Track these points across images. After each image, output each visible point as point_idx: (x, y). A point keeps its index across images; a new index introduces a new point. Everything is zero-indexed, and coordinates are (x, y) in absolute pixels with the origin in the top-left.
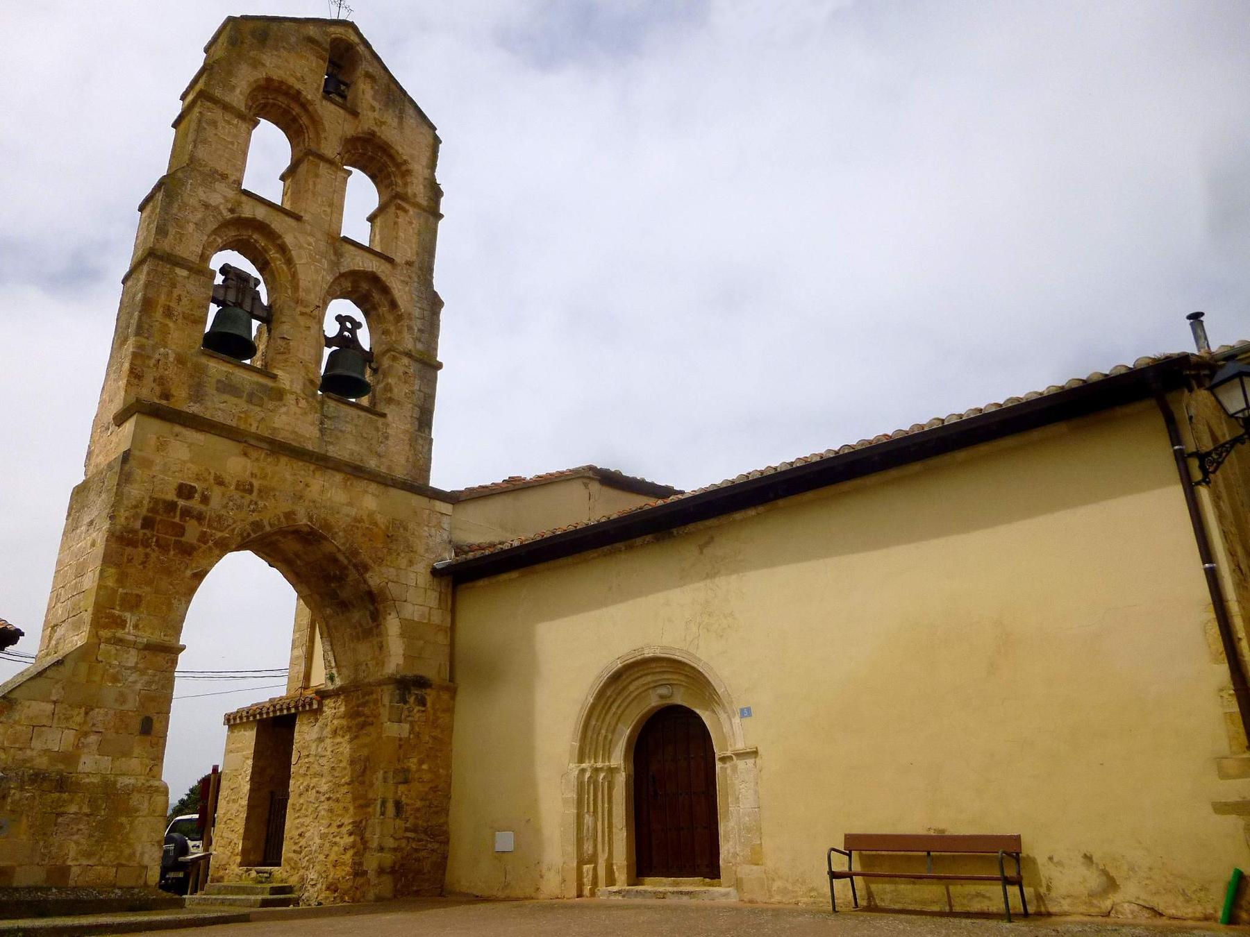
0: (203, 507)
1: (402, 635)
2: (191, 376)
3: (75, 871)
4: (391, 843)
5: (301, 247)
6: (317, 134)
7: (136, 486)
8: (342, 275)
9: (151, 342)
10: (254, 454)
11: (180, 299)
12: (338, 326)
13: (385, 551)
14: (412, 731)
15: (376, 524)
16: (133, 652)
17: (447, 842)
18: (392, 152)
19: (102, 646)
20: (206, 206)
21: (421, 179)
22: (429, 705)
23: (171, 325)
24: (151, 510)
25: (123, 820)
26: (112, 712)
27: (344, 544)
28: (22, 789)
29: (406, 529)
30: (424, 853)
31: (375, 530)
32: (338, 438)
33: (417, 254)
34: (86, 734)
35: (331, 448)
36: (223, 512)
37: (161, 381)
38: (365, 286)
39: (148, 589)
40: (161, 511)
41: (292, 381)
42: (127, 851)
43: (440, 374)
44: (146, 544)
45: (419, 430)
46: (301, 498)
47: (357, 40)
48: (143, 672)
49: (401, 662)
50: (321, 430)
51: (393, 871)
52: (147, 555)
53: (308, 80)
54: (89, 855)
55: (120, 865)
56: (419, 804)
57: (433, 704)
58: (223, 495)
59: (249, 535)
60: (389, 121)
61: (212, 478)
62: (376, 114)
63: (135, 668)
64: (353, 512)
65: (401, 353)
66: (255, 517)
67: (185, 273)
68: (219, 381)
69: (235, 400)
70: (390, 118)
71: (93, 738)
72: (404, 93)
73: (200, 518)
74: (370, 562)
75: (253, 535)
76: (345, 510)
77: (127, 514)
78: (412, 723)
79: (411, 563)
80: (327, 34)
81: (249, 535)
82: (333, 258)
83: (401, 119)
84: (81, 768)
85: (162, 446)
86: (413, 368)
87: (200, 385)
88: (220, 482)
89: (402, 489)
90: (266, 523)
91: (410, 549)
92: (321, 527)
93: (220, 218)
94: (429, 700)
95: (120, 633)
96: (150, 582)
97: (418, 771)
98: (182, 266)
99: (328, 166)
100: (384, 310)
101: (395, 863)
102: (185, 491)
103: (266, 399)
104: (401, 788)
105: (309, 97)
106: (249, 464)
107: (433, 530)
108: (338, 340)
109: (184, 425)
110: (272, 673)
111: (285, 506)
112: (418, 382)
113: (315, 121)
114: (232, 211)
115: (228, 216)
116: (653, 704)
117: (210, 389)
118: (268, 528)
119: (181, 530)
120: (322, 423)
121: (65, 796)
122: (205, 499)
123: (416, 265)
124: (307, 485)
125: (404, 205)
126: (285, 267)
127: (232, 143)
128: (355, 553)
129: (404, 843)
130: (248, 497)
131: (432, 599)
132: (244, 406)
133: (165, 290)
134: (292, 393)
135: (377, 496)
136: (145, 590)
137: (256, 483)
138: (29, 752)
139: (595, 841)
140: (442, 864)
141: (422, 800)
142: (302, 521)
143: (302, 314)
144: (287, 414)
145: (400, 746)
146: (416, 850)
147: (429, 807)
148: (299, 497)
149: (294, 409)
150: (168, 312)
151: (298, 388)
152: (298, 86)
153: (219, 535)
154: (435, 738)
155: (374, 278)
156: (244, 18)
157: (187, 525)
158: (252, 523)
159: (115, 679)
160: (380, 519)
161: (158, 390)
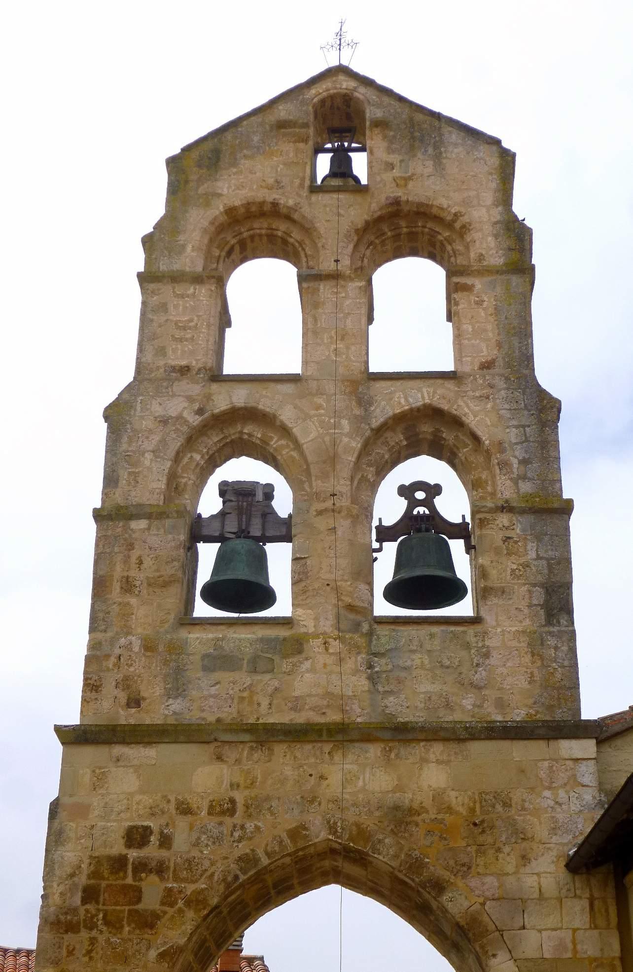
0: (164, 853)
2: (166, 663)
6: (315, 245)
7: (70, 846)
8: (379, 431)
9: (109, 634)
10: (231, 754)
11: (140, 563)
12: (403, 503)
13: (472, 849)
15: (449, 809)
18: (434, 211)
20: (164, 421)
21: (487, 228)
24: (95, 874)
27: (396, 856)
29: (507, 805)
32: (399, 681)
33: (499, 345)
36: (195, 853)
37: (126, 683)
38: (426, 429)
41: (316, 619)
43: (575, 522)
44: (91, 925)
45: (549, 623)
46: (312, 802)
47: (352, 84)
50: (370, 678)
52: (93, 941)
53: (285, 181)
58: (191, 828)
59: (236, 877)
60: (419, 170)
61: (172, 807)
62: (396, 173)
65: (491, 511)
66: (243, 848)
67: (142, 524)
68: (205, 656)
69: (236, 675)
70: (422, 165)
73: (160, 870)
74: (446, 875)
75: (242, 878)
77: (61, 888)
79: (525, 859)
80: (303, 103)
81: (236, 877)
82: (357, 412)
83: (438, 159)
85: (100, 779)
86: (519, 526)
87: (179, 671)
88: (185, 809)
90: (260, 853)
91: (521, 836)
92: (351, 839)
93: (185, 429)
102: (137, 837)
103: (277, 659)
105: (291, 203)
109: (124, 742)
111: (289, 820)
112: (532, 546)
113: (307, 229)
114: (200, 412)
115: (195, 420)
117: (194, 673)
118: (265, 861)
119: (136, 894)
120: (370, 667)
122: (166, 841)
123: (500, 362)
124: (322, 777)
125: (468, 281)
126: (294, 454)
130: (228, 821)
132: (245, 679)
133: (119, 558)
134: (316, 636)
142: (319, 834)
143: (320, 513)
144: (312, 670)
148: (312, 799)
149: (322, 659)
150: (128, 586)
151: (327, 625)
153: (190, 888)
155: (434, 413)
156: (187, 149)
158: (240, 858)
160: (455, 798)
161: (123, 697)
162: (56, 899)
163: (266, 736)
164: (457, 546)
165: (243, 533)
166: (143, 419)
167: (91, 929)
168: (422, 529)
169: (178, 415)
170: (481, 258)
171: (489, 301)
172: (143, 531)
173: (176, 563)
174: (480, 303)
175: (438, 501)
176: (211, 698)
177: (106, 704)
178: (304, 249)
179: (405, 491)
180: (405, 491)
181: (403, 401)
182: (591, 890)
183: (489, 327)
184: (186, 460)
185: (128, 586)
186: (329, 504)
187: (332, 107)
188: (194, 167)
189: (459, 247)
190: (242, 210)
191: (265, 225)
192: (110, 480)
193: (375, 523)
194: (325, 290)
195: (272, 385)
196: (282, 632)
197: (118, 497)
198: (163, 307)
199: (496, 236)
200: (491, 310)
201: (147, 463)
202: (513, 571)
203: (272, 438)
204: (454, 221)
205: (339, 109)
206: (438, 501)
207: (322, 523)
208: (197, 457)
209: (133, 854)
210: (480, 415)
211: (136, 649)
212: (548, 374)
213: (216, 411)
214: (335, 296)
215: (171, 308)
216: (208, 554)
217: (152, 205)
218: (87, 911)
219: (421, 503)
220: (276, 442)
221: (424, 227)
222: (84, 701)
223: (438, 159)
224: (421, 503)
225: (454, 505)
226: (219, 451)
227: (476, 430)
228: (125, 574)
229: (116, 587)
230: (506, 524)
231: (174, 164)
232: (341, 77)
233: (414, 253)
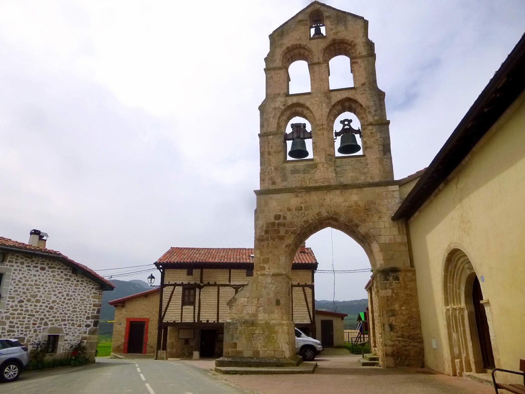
0: (284, 221)
1: (381, 251)
2: (281, 173)
3: (261, 352)
4: (390, 343)
5: (313, 104)
6: (312, 55)
8: (334, 106)
12: (342, 125)
14: (393, 292)
15: (359, 206)
16: (269, 277)
17: (422, 342)
18: (345, 41)
21: (361, 44)
22: (401, 279)
23: (271, 157)
24: (267, 227)
25: (274, 335)
26: (266, 299)
27: (345, 219)
28: (241, 326)
29: (375, 204)
31: (359, 208)
32: (343, 173)
33: (367, 78)
34: (259, 307)
38: (347, 104)
39: (271, 255)
41: (320, 159)
42: (277, 346)
44: (267, 240)
46: (322, 206)
47: (319, 6)
48: (274, 284)
49: (382, 262)
51: (393, 355)
52: (268, 243)
54: (265, 347)
55: (275, 351)
56: (402, 325)
63: (271, 283)
64: (347, 204)
66: (305, 219)
68: (291, 170)
70: (341, 28)
71: (261, 308)
72: (344, 12)
75: (305, 226)
76: (343, 204)
78: (392, 289)
79: (380, 218)
82: (327, 101)
84: (259, 318)
85: (266, 204)
86: (374, 129)
88: (289, 210)
89: (369, 187)
90: (310, 220)
95: (264, 272)
96: (271, 252)
98: (270, 135)
99: (318, 65)
100: (358, 110)
101: (394, 351)
102: (277, 217)
104: (392, 318)
105: (304, 44)
106: (299, 199)
107: (390, 200)
108: (344, 131)
110: (364, 270)
111: (316, 211)
113: (310, 51)
114: (284, 105)
115: (283, 108)
116: (469, 273)
117: (288, 175)
118: (311, 222)
119: (278, 231)
120: (336, 170)
121: (254, 328)
122: (285, 218)
123: (367, 83)
126: (311, 114)
128: (351, 221)
129: (397, 343)
130: (301, 212)
131: (395, 231)
135: (358, 194)
136: (270, 256)
137: (303, 206)
138: (243, 314)
139: (459, 347)
140: (421, 353)
141: (404, 323)
143: (319, 130)
144: (320, 172)
145: (388, 300)
146: (405, 346)
147: (409, 326)
148: (322, 205)
149: (322, 169)
150: (269, 153)
151: (323, 160)
152: (299, 42)
153: (292, 229)
154: (407, 295)
155: (349, 99)
157: (280, 229)
159: (265, 288)
160: (361, 204)
161: (270, 182)
162: (258, 234)
163: (309, 190)
164: (357, 136)
165: (298, 137)
168: (347, 132)
170: (360, 53)
171: (363, 65)
176: (293, 181)
179: (342, 122)
180: (342, 122)
185: (269, 153)
186: (321, 127)
188: (276, 37)
189: (353, 51)
192: (262, 126)
193: (334, 132)
197: (265, 130)
199: (364, 46)
202: (374, 142)
206: (351, 124)
207: (320, 133)
208: (284, 118)
209: (277, 221)
210: (362, 99)
212: (381, 85)
214: (319, 70)
216: (289, 143)
217: (266, 49)
220: (305, 112)
223: (345, 25)
225: (356, 125)
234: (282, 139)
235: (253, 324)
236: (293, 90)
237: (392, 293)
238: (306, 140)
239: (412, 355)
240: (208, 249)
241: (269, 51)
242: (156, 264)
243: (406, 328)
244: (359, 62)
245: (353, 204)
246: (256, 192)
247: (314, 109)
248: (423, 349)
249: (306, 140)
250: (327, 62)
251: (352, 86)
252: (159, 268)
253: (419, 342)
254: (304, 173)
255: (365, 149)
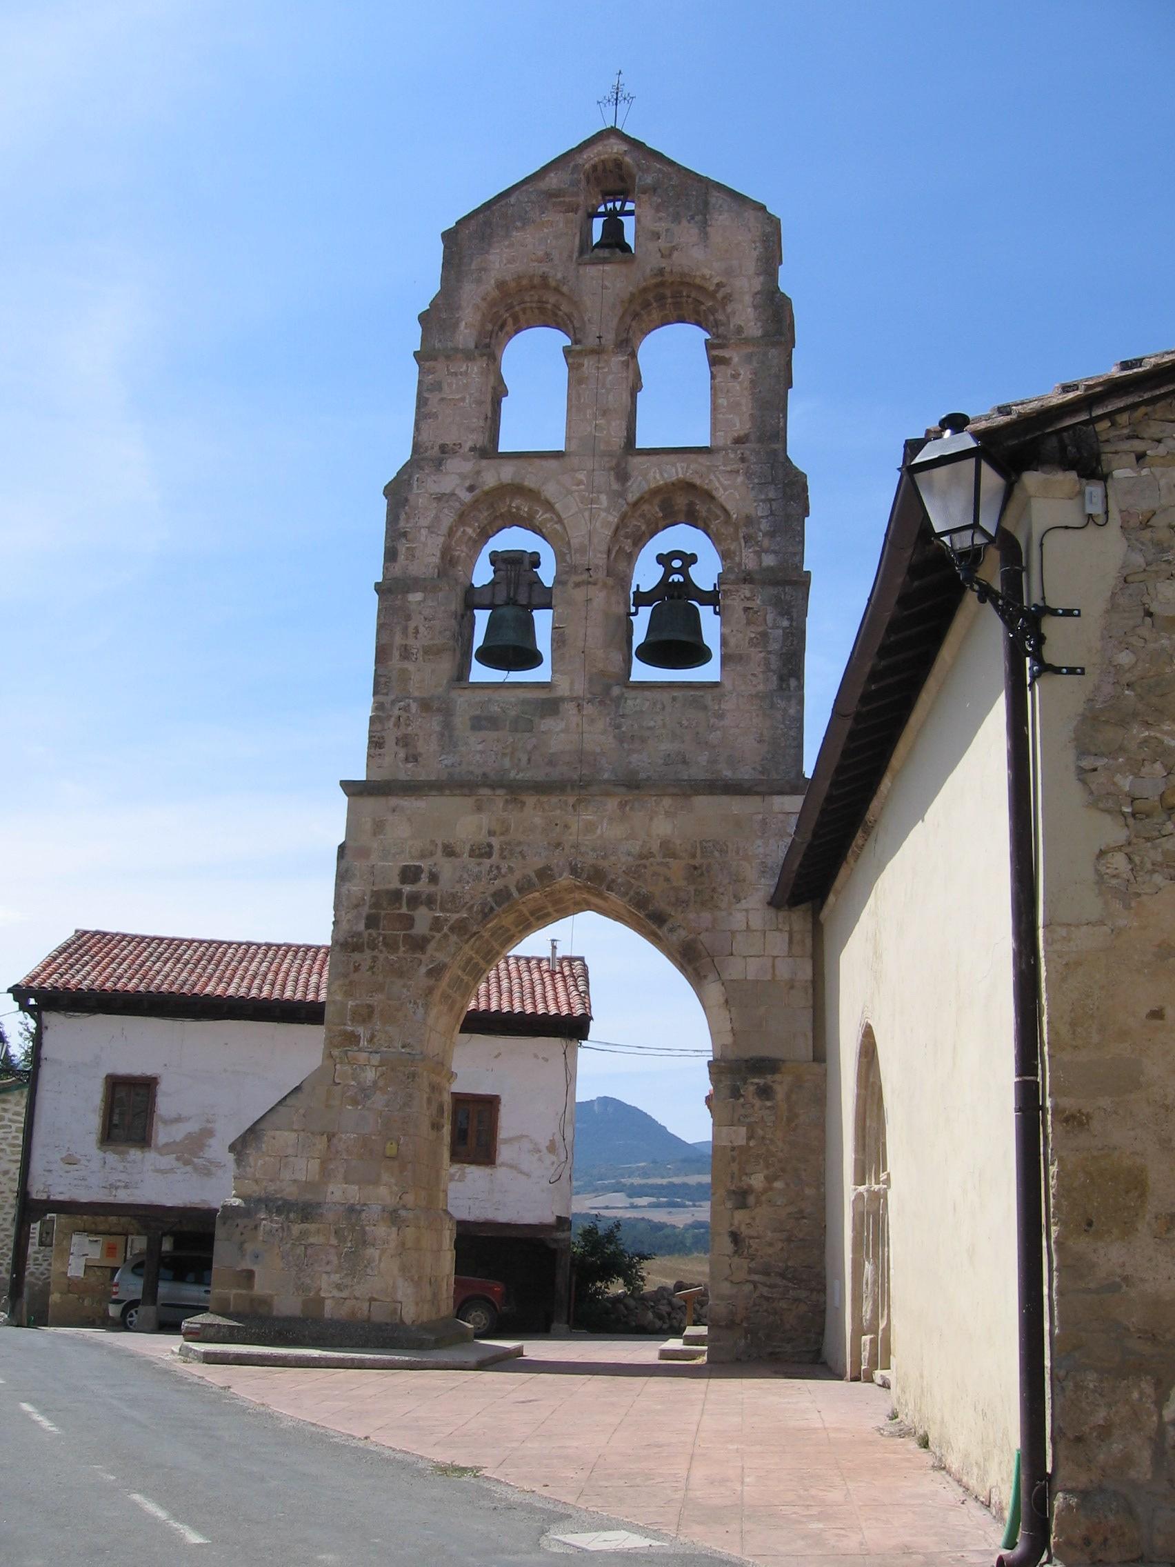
0: (432, 889)
3: (329, 1304)
11: (417, 632)
19: (338, 1067)
20: (439, 498)
21: (748, 299)
24: (376, 905)
30: (783, 1304)
35: (634, 758)
36: (458, 887)
40: (385, 904)
41: (572, 683)
57: (788, 1097)
66: (499, 884)
70: (687, 233)
73: (430, 901)
77: (349, 916)
82: (616, 486)
85: (379, 827)
88: (449, 852)
94: (780, 1092)
97: (765, 1191)
102: (411, 874)
104: (740, 1216)
114: (471, 489)
115: (466, 497)
119: (409, 922)
122: (434, 878)
124: (566, 826)
126: (558, 527)
127: (463, 399)
130: (487, 862)
131: (778, 943)
137: (495, 842)
141: (774, 1231)
143: (577, 585)
150: (406, 653)
151: (580, 688)
153: (456, 916)
155: (688, 487)
162: (345, 926)
163: (515, 790)
164: (706, 614)
165: (511, 602)
166: (420, 496)
167: (373, 949)
168: (676, 598)
169: (449, 491)
170: (739, 330)
171: (745, 373)
172: (419, 603)
173: (448, 633)
174: (735, 376)
175: (693, 570)
176: (477, 751)
177: (388, 760)
178: (572, 322)
179: (663, 559)
180: (663, 559)
181: (658, 476)
182: (790, 925)
183: (743, 401)
184: (459, 533)
185: (406, 653)
186: (585, 577)
187: (604, 170)
188: (464, 242)
189: (720, 316)
190: (513, 285)
191: (536, 298)
192: (391, 555)
193: (634, 589)
194: (588, 363)
195: (537, 462)
196: (542, 694)
197: (397, 570)
198: (437, 387)
199: (755, 307)
200: (746, 384)
201: (423, 539)
202: (751, 639)
203: (537, 512)
204: (716, 291)
205: (610, 176)
206: (693, 570)
207: (579, 595)
208: (469, 531)
209: (407, 889)
210: (733, 492)
211: (414, 711)
212: (799, 450)
213: (486, 488)
215: (445, 386)
216: (482, 618)
218: (370, 935)
219: (677, 571)
220: (541, 516)
221: (688, 297)
222: (369, 756)
223: (704, 226)
224: (677, 571)
225: (705, 575)
226: (490, 523)
227: (724, 504)
228: (404, 642)
229: (396, 654)
230: (748, 595)
231: (449, 237)
232: (613, 140)
233: (681, 320)
234: (455, 605)
235: (307, 1211)
236: (515, 435)
237: (749, 1138)
238: (536, 613)
239: (788, 1327)
240: (211, 943)
241: (790, 454)
242: (19, 993)
243: (780, 1245)
244: (736, 360)
245: (655, 847)
246: (349, 787)
247: (568, 507)
248: (824, 1311)
249: (536, 613)
250: (627, 346)
251: (706, 443)
252: (24, 1007)
253: (812, 1290)
254: (515, 730)
255: (725, 660)
